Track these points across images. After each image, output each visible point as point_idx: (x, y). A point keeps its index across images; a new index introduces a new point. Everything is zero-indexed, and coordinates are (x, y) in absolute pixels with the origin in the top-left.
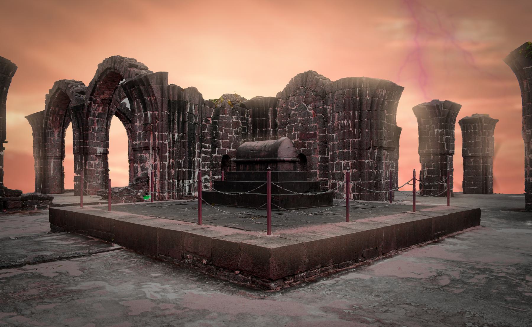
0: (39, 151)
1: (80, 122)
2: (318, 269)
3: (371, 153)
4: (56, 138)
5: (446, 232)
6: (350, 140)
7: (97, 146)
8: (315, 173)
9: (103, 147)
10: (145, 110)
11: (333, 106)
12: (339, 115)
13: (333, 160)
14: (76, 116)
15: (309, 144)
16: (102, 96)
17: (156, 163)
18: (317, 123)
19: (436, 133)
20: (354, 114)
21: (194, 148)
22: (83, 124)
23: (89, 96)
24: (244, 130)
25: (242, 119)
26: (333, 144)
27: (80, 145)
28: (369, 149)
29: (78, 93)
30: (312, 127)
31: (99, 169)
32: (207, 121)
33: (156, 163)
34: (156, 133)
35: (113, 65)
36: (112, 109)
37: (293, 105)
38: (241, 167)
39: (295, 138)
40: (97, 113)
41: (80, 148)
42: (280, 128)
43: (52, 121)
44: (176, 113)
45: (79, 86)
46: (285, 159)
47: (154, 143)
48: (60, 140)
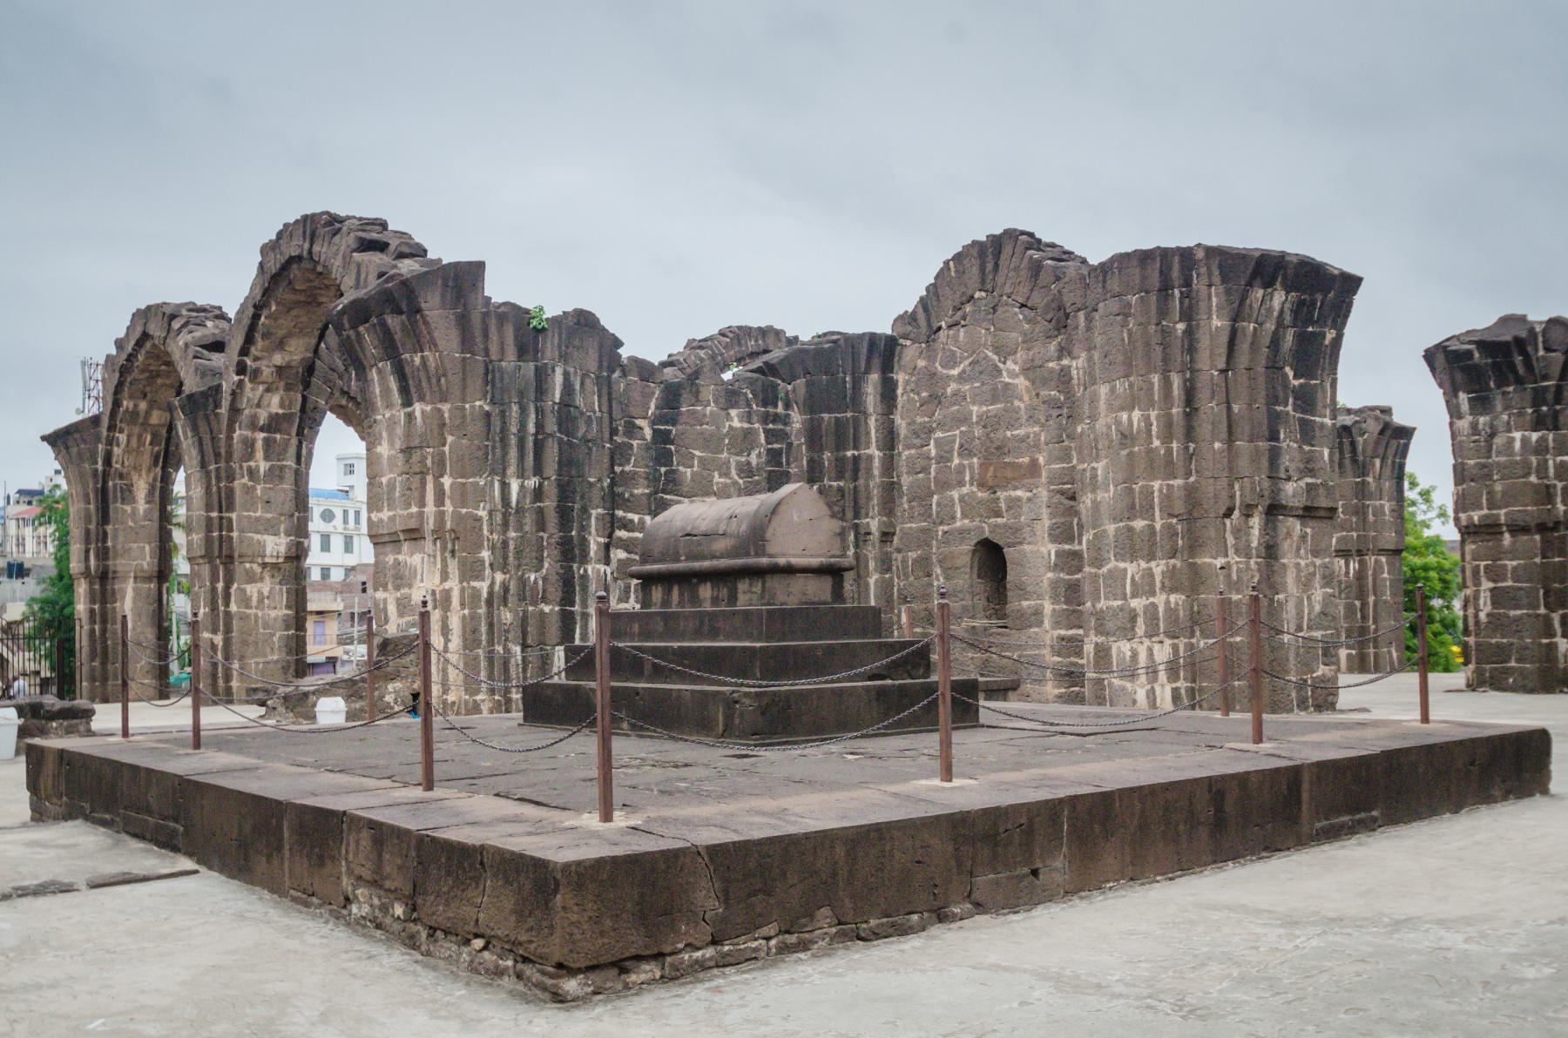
0: (87, 551)
1: (208, 448)
2: (768, 939)
3: (1236, 532)
4: (142, 506)
5: (1375, 820)
6: (1156, 484)
7: (266, 531)
8: (1038, 612)
9: (288, 534)
10: (407, 403)
11: (1090, 359)
12: (1113, 390)
13: (1098, 562)
14: (195, 428)
15: (1014, 504)
16: (278, 359)
17: (447, 585)
18: (1037, 422)
19: (1517, 445)
20: (1167, 384)
21: (583, 528)
22: (217, 455)
23: (236, 358)
24: (774, 456)
25: (765, 419)
26: (1094, 502)
27: (209, 529)
28: (1229, 513)
29: (203, 347)
30: (1023, 439)
31: (273, 614)
32: (632, 430)
33: (447, 585)
34: (447, 481)
35: (307, 246)
36: (313, 394)
37: (951, 361)
38: (657, 594)
39: (961, 483)
40: (263, 417)
41: (208, 540)
42: (908, 447)
43: (128, 450)
44: (515, 408)
45: (209, 324)
46: (794, 561)
47: (440, 516)
48: (156, 514)
